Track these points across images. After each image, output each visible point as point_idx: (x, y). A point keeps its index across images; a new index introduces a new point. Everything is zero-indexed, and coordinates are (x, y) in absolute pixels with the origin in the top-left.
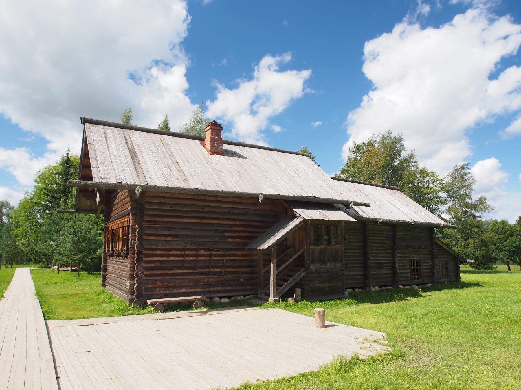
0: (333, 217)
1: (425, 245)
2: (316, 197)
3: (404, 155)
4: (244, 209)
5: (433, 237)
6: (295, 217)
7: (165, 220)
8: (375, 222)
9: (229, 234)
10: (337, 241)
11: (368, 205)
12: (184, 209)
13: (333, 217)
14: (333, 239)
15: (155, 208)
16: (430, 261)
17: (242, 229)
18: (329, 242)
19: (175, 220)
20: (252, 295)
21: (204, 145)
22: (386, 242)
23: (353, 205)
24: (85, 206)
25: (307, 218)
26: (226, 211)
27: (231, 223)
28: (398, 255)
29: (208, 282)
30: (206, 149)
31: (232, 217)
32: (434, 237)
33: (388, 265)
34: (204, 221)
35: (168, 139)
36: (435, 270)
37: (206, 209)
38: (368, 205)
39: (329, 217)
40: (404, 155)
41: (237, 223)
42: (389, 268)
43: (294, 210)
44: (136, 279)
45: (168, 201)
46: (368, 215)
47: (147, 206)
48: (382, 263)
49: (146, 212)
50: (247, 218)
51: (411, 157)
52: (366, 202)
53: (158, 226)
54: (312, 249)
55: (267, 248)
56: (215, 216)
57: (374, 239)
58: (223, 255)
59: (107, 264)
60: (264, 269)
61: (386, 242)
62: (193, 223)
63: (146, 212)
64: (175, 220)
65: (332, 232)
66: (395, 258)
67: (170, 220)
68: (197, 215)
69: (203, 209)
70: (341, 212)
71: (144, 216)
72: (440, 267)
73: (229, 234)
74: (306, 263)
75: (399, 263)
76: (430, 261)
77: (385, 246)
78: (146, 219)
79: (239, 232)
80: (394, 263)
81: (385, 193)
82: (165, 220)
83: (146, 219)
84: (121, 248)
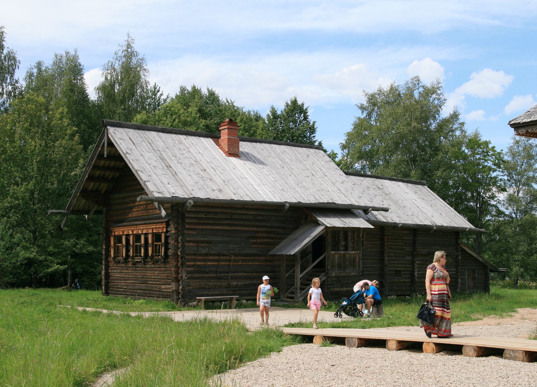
0: (352, 224)
1: (449, 251)
2: (335, 203)
3: (445, 113)
4: (267, 215)
5: (458, 242)
6: (318, 224)
7: (201, 227)
8: (394, 226)
9: (254, 241)
10: (354, 247)
11: (386, 210)
12: (216, 217)
13: (352, 224)
14: (350, 245)
15: (192, 216)
16: (454, 269)
17: (265, 235)
18: (346, 248)
19: (208, 227)
20: (275, 299)
21: (218, 144)
22: (405, 247)
23: (371, 210)
24: (79, 206)
25: (329, 225)
26: (251, 217)
27: (255, 229)
28: (417, 262)
29: (237, 285)
30: (221, 148)
31: (257, 224)
32: (459, 242)
33: (407, 272)
34: (232, 228)
35: (184, 139)
36: (459, 280)
37: (234, 217)
38: (386, 210)
39: (349, 224)
40: (445, 113)
41: (260, 229)
42: (408, 276)
43: (319, 219)
44: (181, 281)
45: (202, 209)
46: (386, 220)
47: (187, 215)
48: (400, 271)
49: (187, 221)
50: (269, 225)
51: (455, 116)
52: (385, 206)
53: (195, 233)
54: (333, 254)
55: (294, 254)
56: (242, 223)
57: (392, 245)
58: (218, 261)
59: (110, 271)
60: (286, 274)
61: (405, 247)
62: (223, 230)
63: (187, 221)
64: (208, 227)
65: (350, 238)
66: (414, 265)
67: (204, 227)
68: (226, 222)
69: (232, 216)
70: (361, 219)
71: (185, 225)
72: (466, 277)
73: (254, 241)
74: (326, 268)
75: (418, 271)
76: (454, 269)
77: (404, 252)
78: (187, 226)
79: (264, 238)
80: (413, 271)
81: (407, 191)
82: (201, 227)
83: (187, 226)
84: (152, 254)
